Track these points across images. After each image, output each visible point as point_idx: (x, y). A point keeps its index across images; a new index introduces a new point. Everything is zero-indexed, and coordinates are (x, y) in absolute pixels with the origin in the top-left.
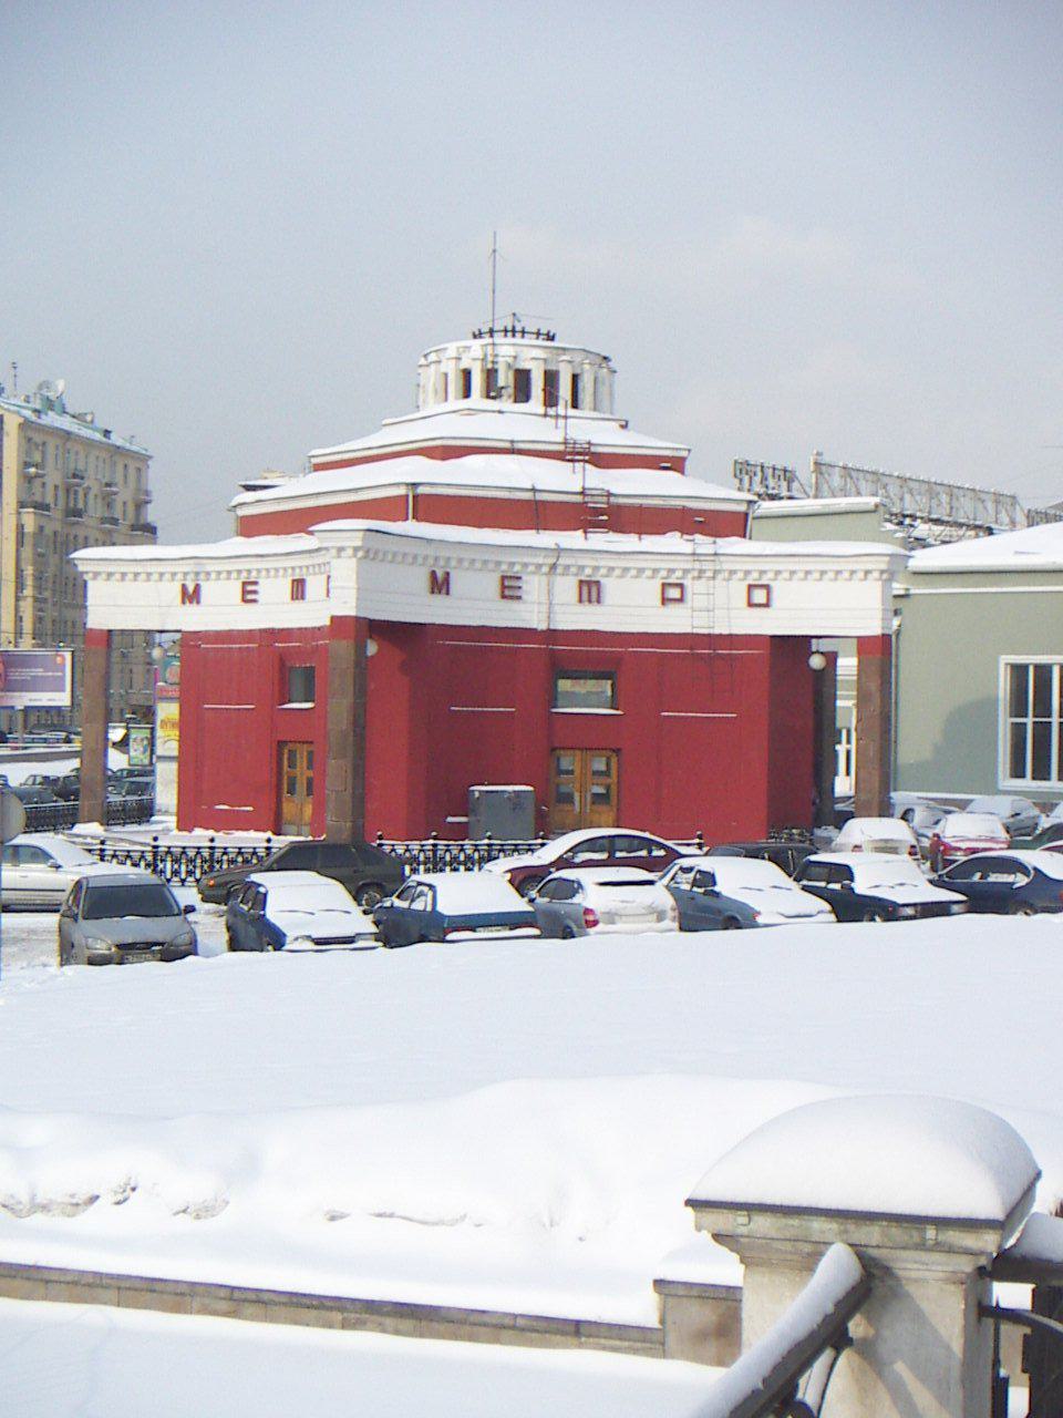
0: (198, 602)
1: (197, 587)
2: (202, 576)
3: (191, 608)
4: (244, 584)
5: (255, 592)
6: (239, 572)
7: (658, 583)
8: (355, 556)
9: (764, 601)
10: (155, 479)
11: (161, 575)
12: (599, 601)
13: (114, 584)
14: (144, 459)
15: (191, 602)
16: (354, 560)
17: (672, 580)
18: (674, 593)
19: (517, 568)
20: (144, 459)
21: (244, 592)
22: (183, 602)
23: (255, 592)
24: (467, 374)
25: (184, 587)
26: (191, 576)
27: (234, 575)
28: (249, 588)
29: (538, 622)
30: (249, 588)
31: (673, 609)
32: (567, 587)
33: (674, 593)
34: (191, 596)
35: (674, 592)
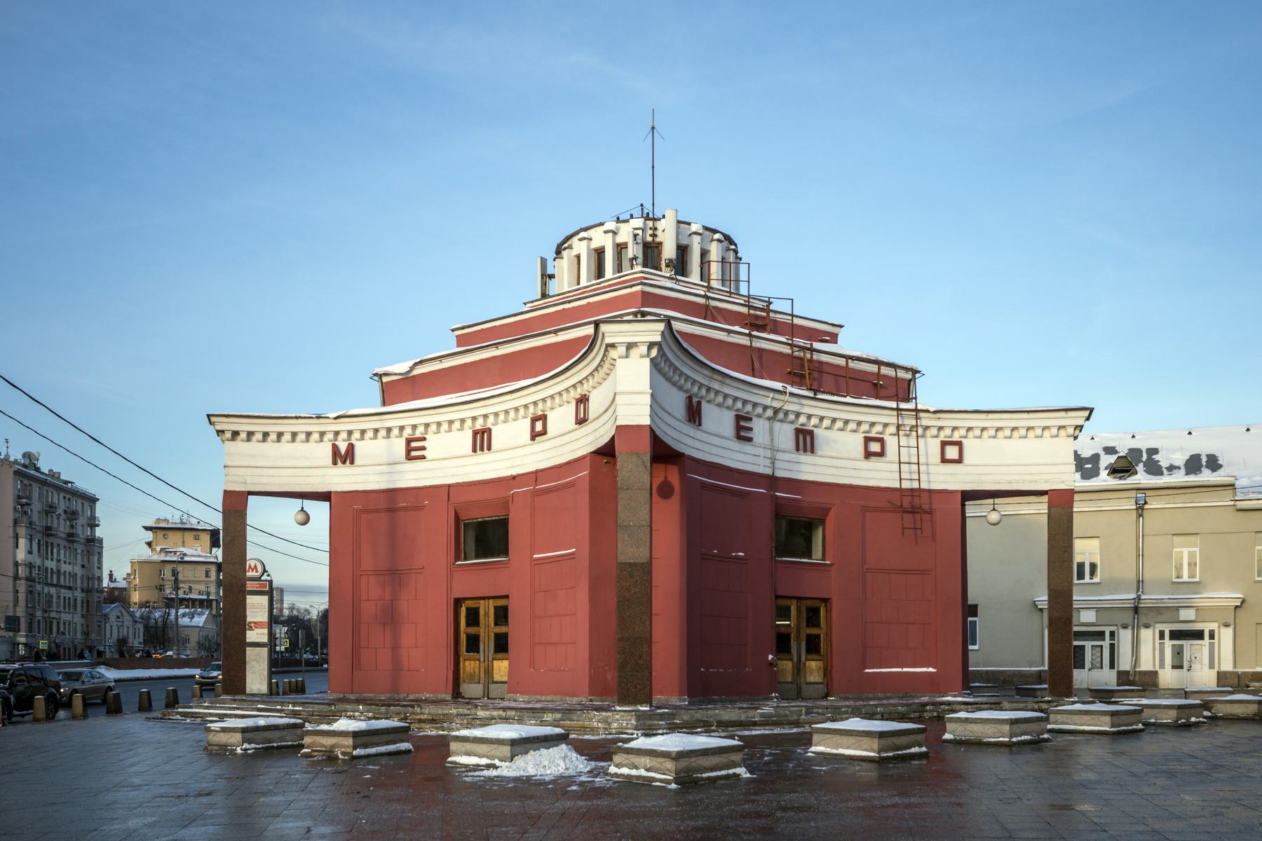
0: (352, 463)
1: (351, 448)
2: (357, 435)
3: (343, 470)
4: (409, 441)
5: (424, 448)
6: (402, 428)
7: (859, 438)
8: (648, 355)
9: (956, 457)
10: (100, 510)
11: (309, 434)
12: (812, 452)
13: (986, 442)
14: (93, 500)
15: (344, 463)
16: (647, 361)
17: (873, 435)
18: (875, 447)
19: (749, 408)
20: (93, 500)
21: (409, 450)
22: (335, 463)
23: (424, 448)
24: (600, 253)
25: (335, 449)
26: (344, 435)
27: (396, 432)
28: (414, 444)
29: (763, 468)
30: (414, 444)
31: (874, 463)
32: (785, 434)
33: (875, 447)
34: (344, 457)
35: (873, 449)
